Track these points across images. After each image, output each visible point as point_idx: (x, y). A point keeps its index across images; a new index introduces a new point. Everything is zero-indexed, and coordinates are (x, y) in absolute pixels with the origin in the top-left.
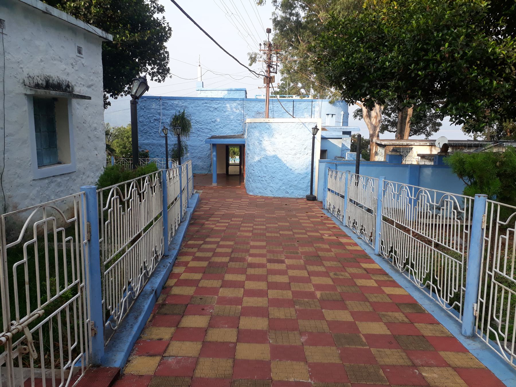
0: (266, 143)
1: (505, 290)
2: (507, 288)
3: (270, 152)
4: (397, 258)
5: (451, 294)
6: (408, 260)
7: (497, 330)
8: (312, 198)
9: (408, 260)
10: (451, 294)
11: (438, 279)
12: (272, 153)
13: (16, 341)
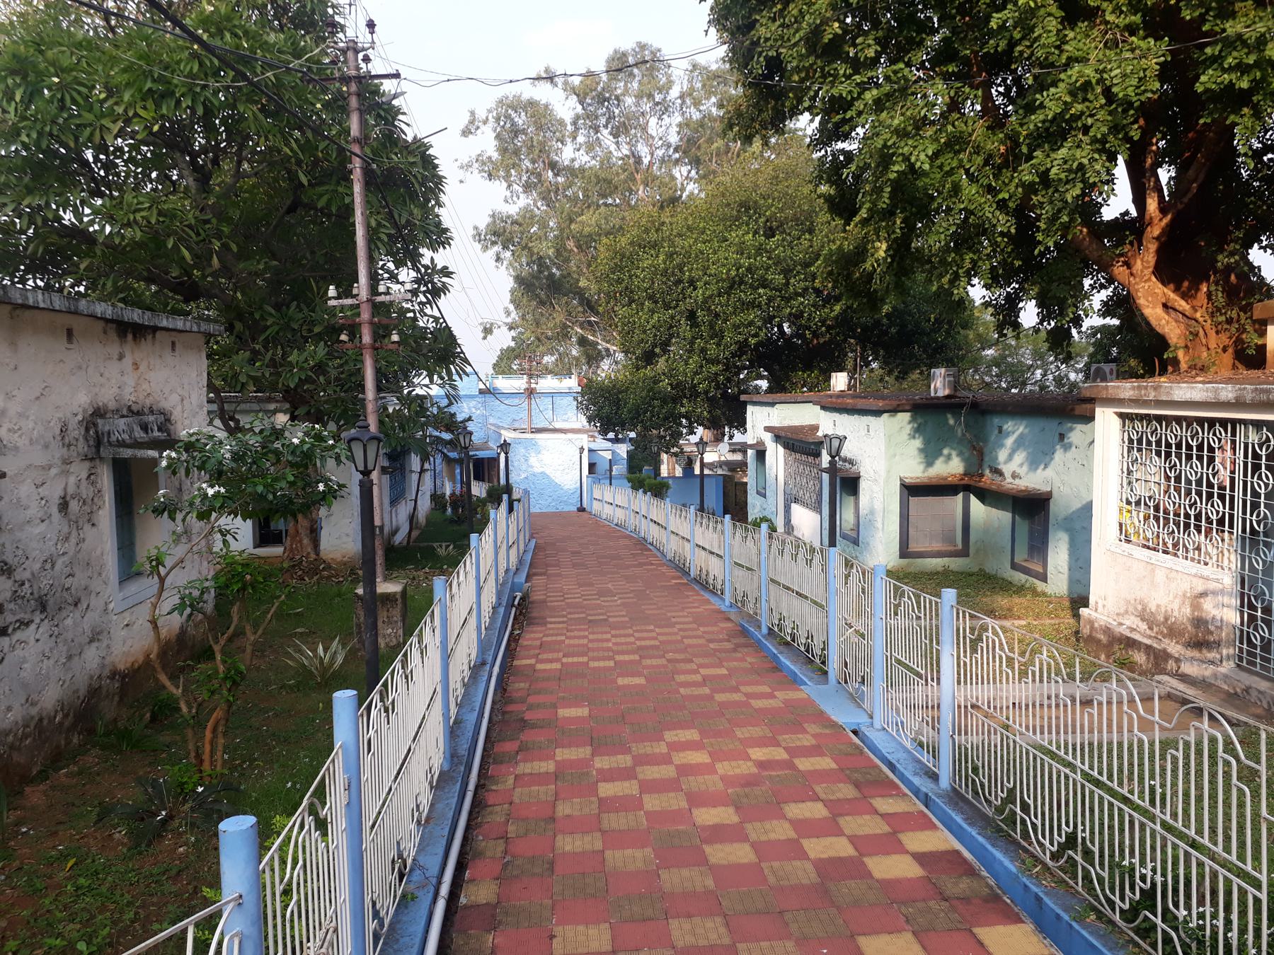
0: (533, 460)
1: (1173, 844)
2: (1122, 806)
3: (538, 470)
4: (1032, 823)
5: (1060, 835)
6: (1011, 792)
7: (1093, 865)
8: (582, 509)
9: (1011, 792)
10: (1060, 835)
11: (1031, 802)
12: (541, 470)
13: (170, 938)
